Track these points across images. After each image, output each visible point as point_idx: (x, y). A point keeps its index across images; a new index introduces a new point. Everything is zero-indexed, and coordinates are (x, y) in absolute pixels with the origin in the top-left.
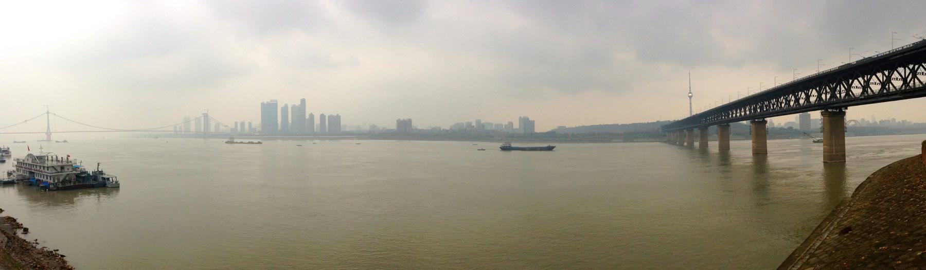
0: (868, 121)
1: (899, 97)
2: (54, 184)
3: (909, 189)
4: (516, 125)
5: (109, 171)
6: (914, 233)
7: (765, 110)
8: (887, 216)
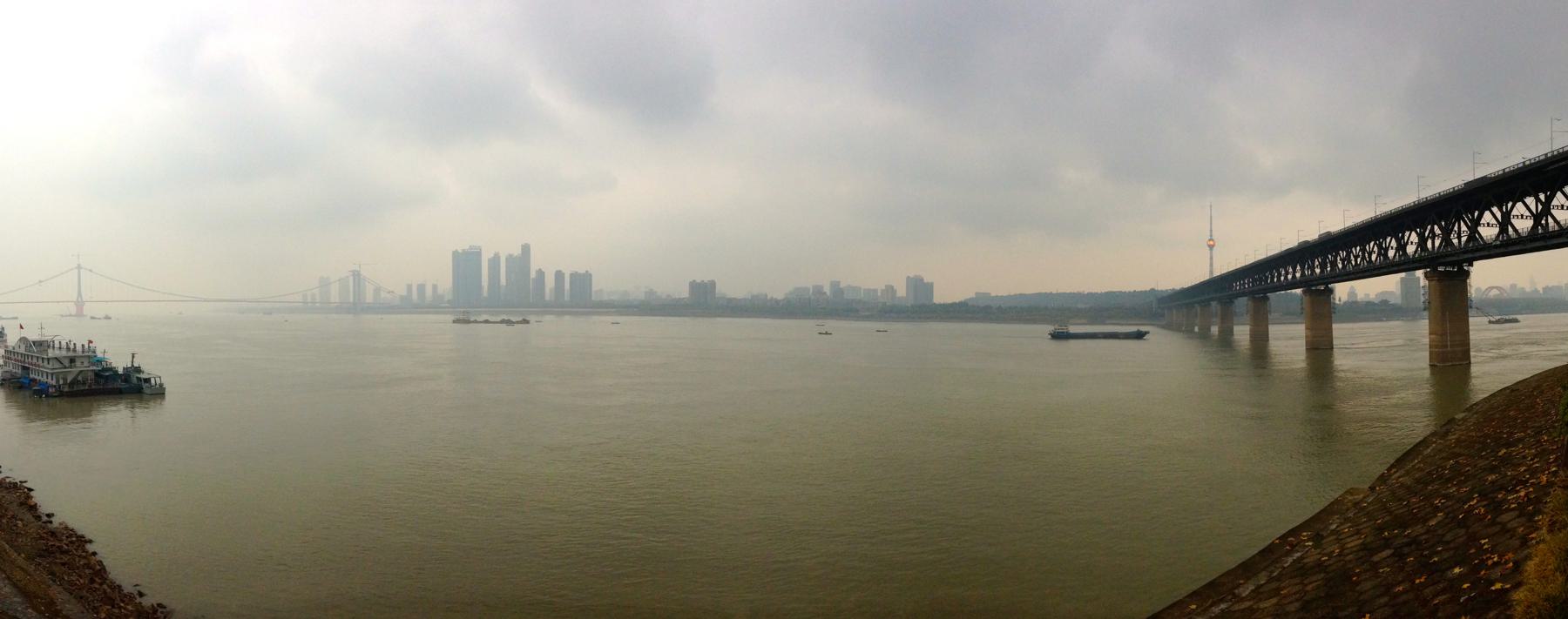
0: (1523, 288)
2: (55, 386)
4: (901, 291)
5: (151, 367)
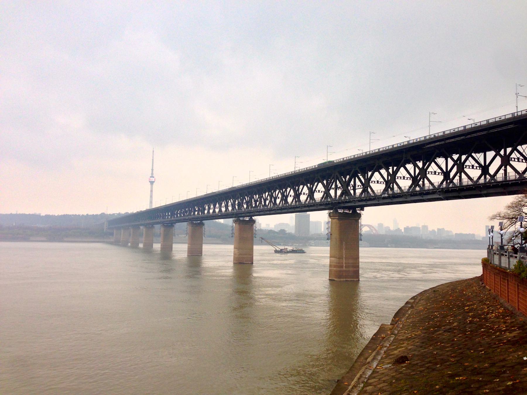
1: (438, 196)
3: (475, 318)
6: (497, 365)
7: (254, 205)
8: (454, 347)
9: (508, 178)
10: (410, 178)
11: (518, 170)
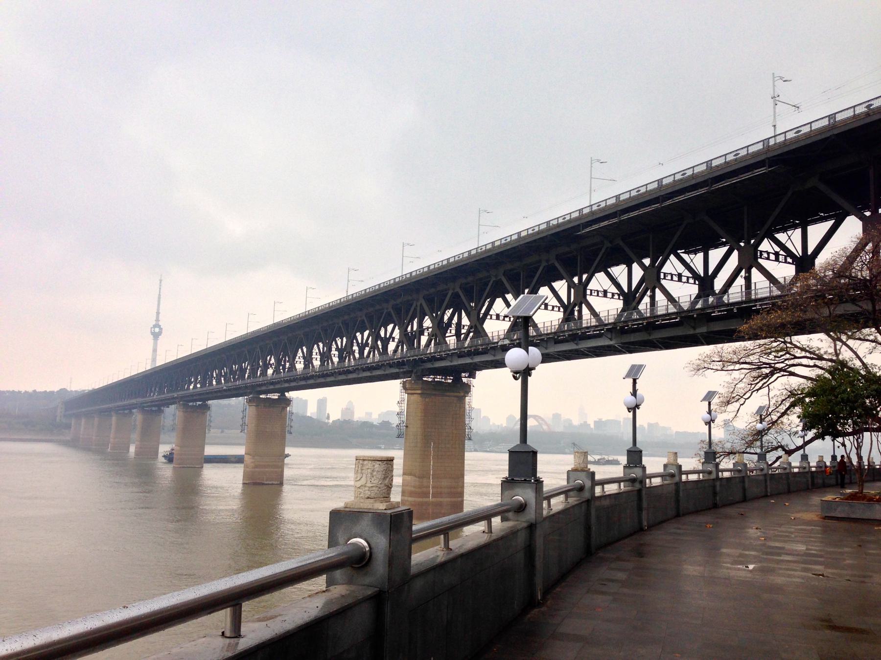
9: (753, 292)
10: (559, 307)
11: (777, 277)
